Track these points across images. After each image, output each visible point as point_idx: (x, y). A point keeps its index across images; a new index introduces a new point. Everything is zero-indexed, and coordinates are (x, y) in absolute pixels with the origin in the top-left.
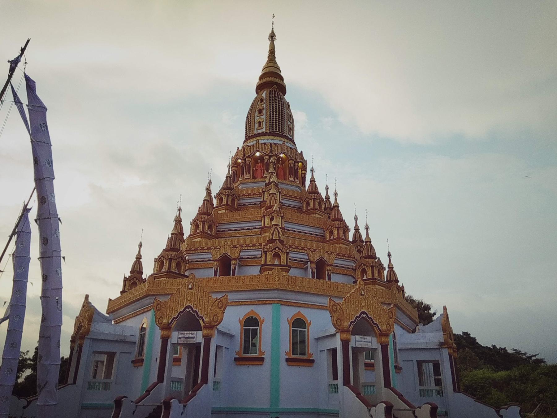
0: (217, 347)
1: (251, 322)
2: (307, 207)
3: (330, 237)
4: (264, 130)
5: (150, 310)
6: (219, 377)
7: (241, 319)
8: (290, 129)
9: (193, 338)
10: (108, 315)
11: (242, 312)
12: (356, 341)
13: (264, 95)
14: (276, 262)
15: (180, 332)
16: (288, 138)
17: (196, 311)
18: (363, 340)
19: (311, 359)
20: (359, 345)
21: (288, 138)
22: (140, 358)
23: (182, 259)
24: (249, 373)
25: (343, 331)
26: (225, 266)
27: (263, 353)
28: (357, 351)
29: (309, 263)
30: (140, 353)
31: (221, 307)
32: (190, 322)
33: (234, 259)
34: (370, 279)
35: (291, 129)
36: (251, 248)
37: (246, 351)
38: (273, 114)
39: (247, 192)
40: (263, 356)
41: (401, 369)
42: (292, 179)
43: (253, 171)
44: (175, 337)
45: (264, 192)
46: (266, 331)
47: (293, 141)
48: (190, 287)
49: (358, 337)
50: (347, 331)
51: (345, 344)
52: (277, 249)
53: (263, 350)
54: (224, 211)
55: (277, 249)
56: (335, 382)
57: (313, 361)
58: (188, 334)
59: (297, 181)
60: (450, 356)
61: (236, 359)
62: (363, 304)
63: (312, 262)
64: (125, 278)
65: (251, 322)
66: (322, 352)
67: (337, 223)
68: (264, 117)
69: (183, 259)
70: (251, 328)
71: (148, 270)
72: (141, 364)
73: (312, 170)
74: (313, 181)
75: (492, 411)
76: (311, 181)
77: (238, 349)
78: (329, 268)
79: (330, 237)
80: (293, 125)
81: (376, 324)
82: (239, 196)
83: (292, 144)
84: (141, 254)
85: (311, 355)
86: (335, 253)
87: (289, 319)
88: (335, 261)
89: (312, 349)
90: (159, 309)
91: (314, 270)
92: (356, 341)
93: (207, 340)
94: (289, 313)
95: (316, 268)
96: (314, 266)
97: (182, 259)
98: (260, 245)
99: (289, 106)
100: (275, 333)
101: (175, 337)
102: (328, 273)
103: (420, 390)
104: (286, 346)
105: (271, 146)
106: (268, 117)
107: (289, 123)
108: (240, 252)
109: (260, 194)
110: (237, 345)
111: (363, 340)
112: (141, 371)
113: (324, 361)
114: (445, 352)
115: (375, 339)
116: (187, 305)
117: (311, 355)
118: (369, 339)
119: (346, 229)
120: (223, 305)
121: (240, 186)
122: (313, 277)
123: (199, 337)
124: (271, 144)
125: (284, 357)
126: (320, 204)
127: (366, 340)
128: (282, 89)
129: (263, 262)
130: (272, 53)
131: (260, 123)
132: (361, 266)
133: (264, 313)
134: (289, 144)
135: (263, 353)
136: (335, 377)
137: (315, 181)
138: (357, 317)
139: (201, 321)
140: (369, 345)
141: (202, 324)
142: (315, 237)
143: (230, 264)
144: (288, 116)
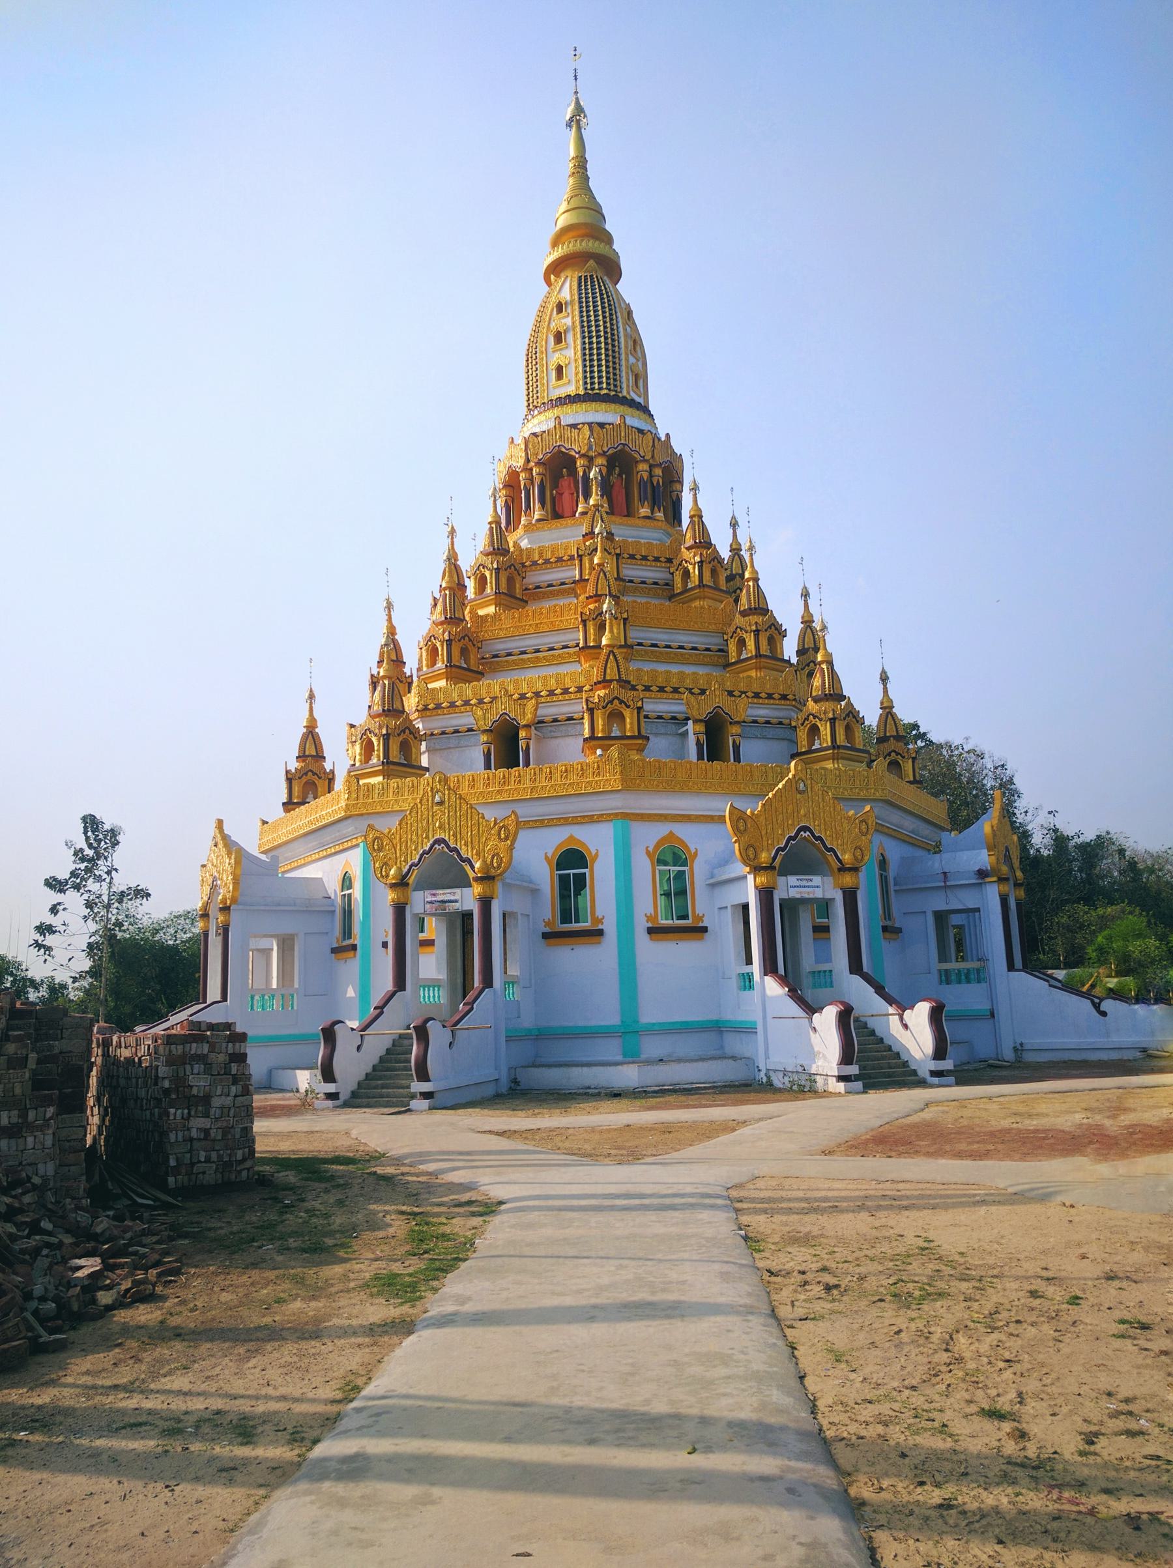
0: (504, 915)
1: (572, 861)
2: (685, 582)
3: (740, 653)
4: (571, 390)
5: (357, 845)
6: (513, 971)
7: (549, 855)
8: (637, 377)
9: (456, 901)
10: (263, 857)
11: (553, 840)
12: (791, 887)
13: (566, 294)
14: (616, 732)
15: (427, 892)
16: (632, 404)
17: (455, 850)
18: (804, 883)
19: (701, 924)
20: (794, 893)
21: (632, 404)
22: (348, 942)
23: (411, 733)
24: (573, 960)
25: (757, 869)
26: (507, 747)
27: (600, 921)
28: (791, 907)
29: (690, 722)
30: (347, 932)
31: (506, 838)
32: (446, 869)
33: (527, 726)
34: (827, 749)
35: (640, 378)
36: (561, 698)
37: (566, 918)
38: (591, 355)
39: (541, 554)
40: (600, 927)
41: (898, 931)
42: (644, 511)
43: (553, 499)
44: (419, 901)
45: (580, 557)
46: (603, 877)
47: (645, 410)
48: (437, 799)
49: (793, 880)
50: (771, 868)
51: (766, 895)
52: (616, 702)
53: (599, 913)
54: (491, 610)
55: (616, 702)
56: (747, 969)
57: (704, 930)
58: (443, 894)
59: (660, 515)
60: (1004, 900)
61: (546, 936)
62: (802, 812)
63: (696, 721)
64: (287, 772)
65: (572, 861)
66: (723, 911)
67: (754, 619)
68: (570, 353)
69: (414, 732)
70: (572, 872)
71: (340, 756)
72: (351, 953)
73: (695, 489)
74: (697, 516)
75: (1086, 1004)
76: (691, 517)
77: (548, 915)
78: (735, 730)
79: (740, 653)
80: (645, 364)
81: (831, 850)
82: (523, 565)
83: (643, 416)
84: (316, 715)
85: (701, 919)
86: (750, 694)
87: (651, 849)
88: (750, 712)
89: (702, 905)
90: (376, 845)
91: (703, 738)
92: (791, 887)
93: (485, 904)
94: (649, 835)
95: (707, 733)
96: (701, 728)
97: (411, 733)
98: (580, 689)
99: (630, 313)
100: (620, 886)
101: (419, 901)
102: (734, 742)
103: (940, 971)
104: (647, 903)
105: (591, 431)
106: (579, 354)
107: (632, 360)
108: (536, 709)
109: (572, 558)
110: (547, 910)
111: (804, 883)
112: (352, 967)
113: (726, 930)
114: (992, 894)
115: (829, 880)
116: (438, 837)
117: (701, 919)
118: (817, 880)
119: (776, 632)
120: (508, 833)
121: (520, 540)
122: (700, 757)
123: (467, 899)
124: (590, 424)
125: (642, 924)
126: (714, 572)
127: (810, 884)
128: (611, 268)
129: (587, 734)
130: (581, 164)
131: (559, 369)
132: (807, 719)
133: (599, 841)
134: (634, 420)
135: (600, 921)
136: (749, 962)
137: (701, 517)
138: (790, 838)
139: (468, 868)
140: (819, 894)
141: (471, 874)
142: (704, 656)
143: (515, 738)
144: (630, 343)
